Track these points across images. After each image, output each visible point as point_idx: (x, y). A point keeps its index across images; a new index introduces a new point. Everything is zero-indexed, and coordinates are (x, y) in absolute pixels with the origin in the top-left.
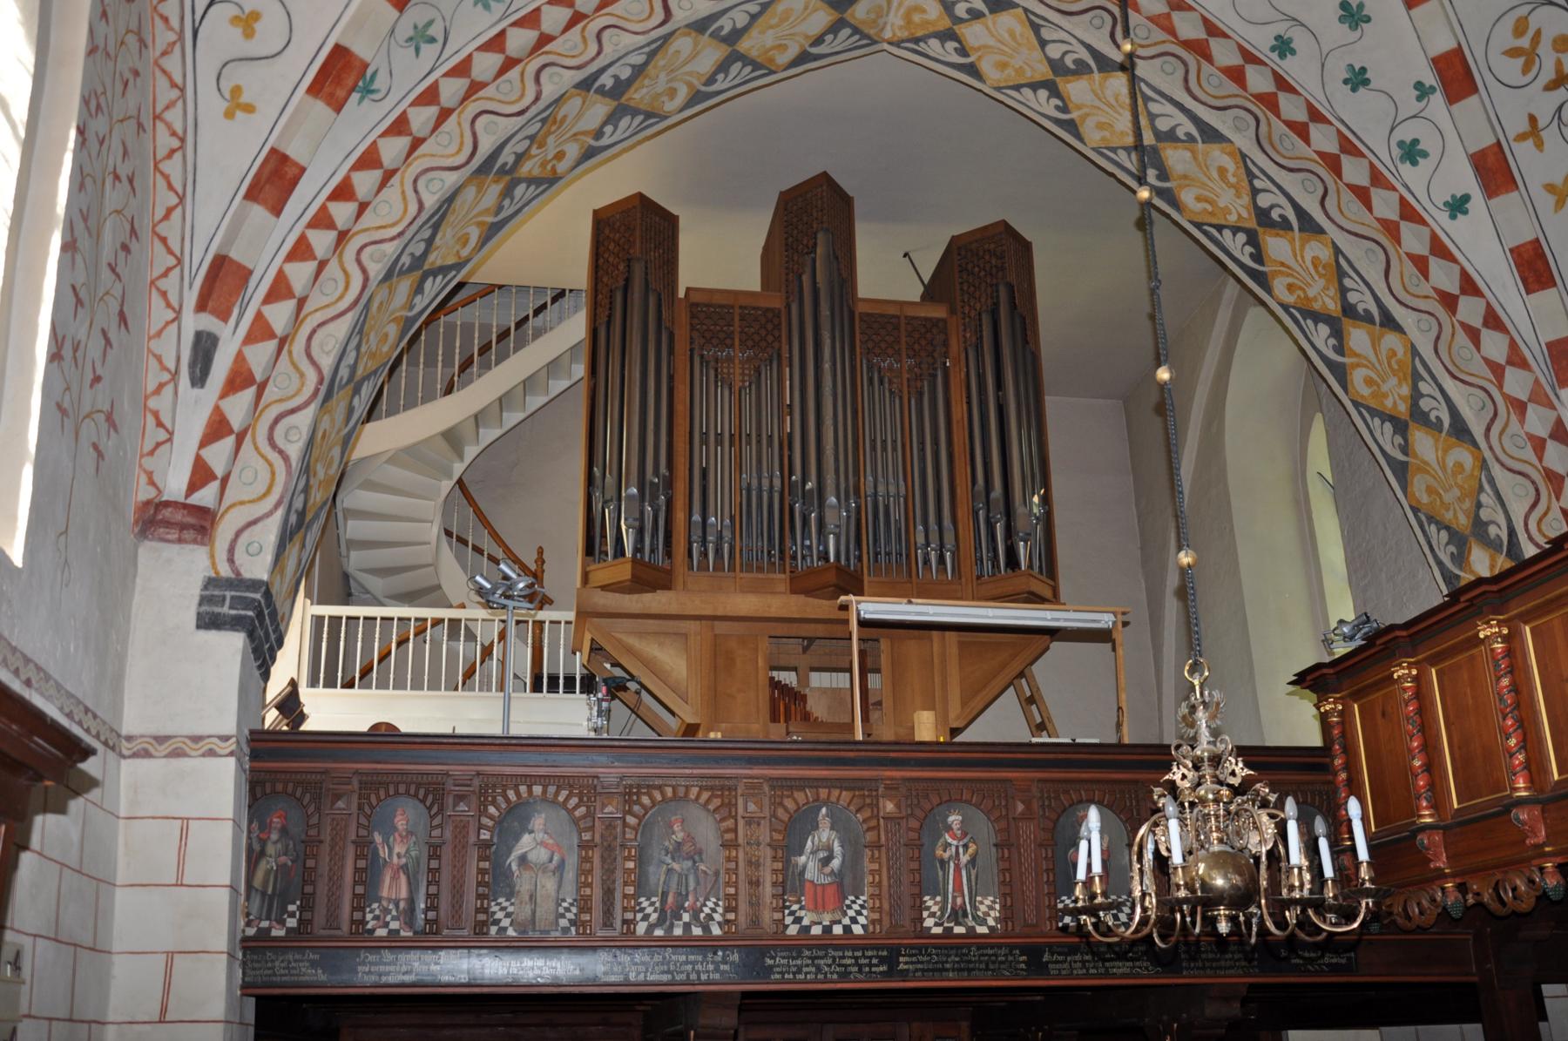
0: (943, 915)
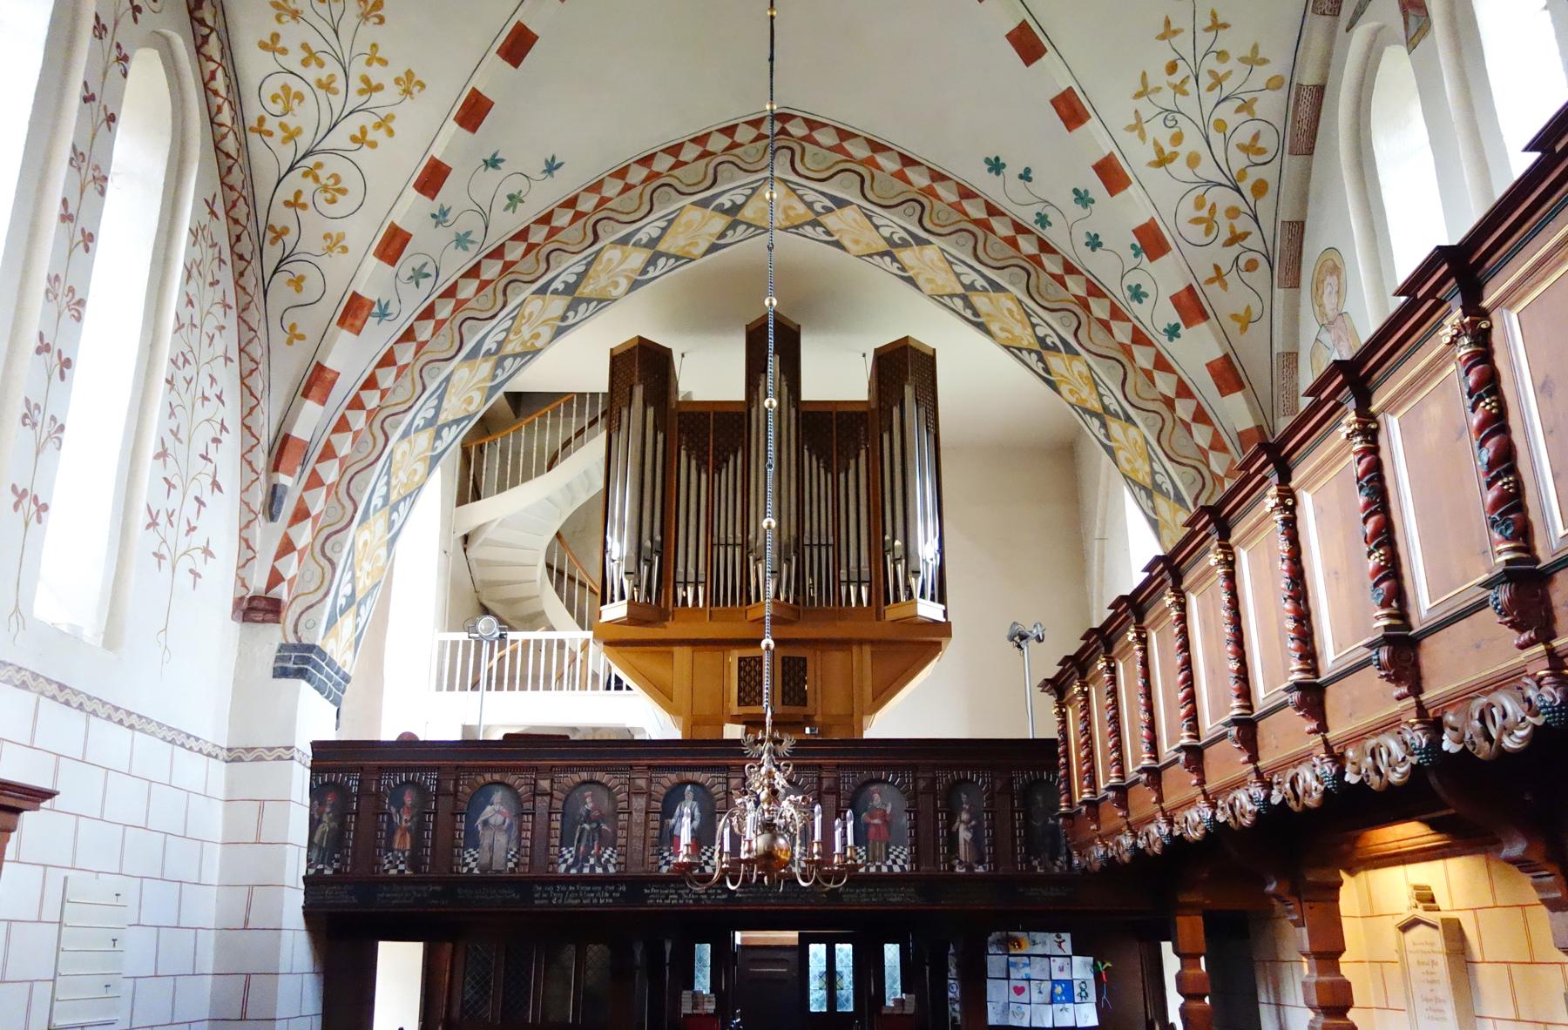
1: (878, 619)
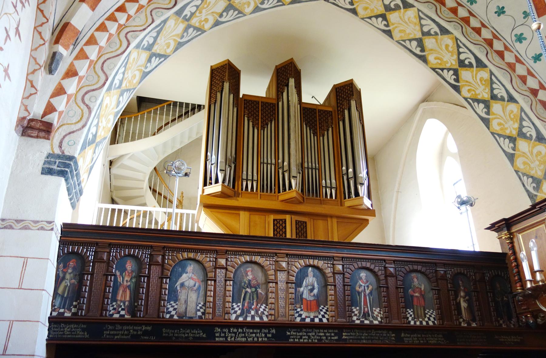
0: (360, 315)
1: (341, 205)
